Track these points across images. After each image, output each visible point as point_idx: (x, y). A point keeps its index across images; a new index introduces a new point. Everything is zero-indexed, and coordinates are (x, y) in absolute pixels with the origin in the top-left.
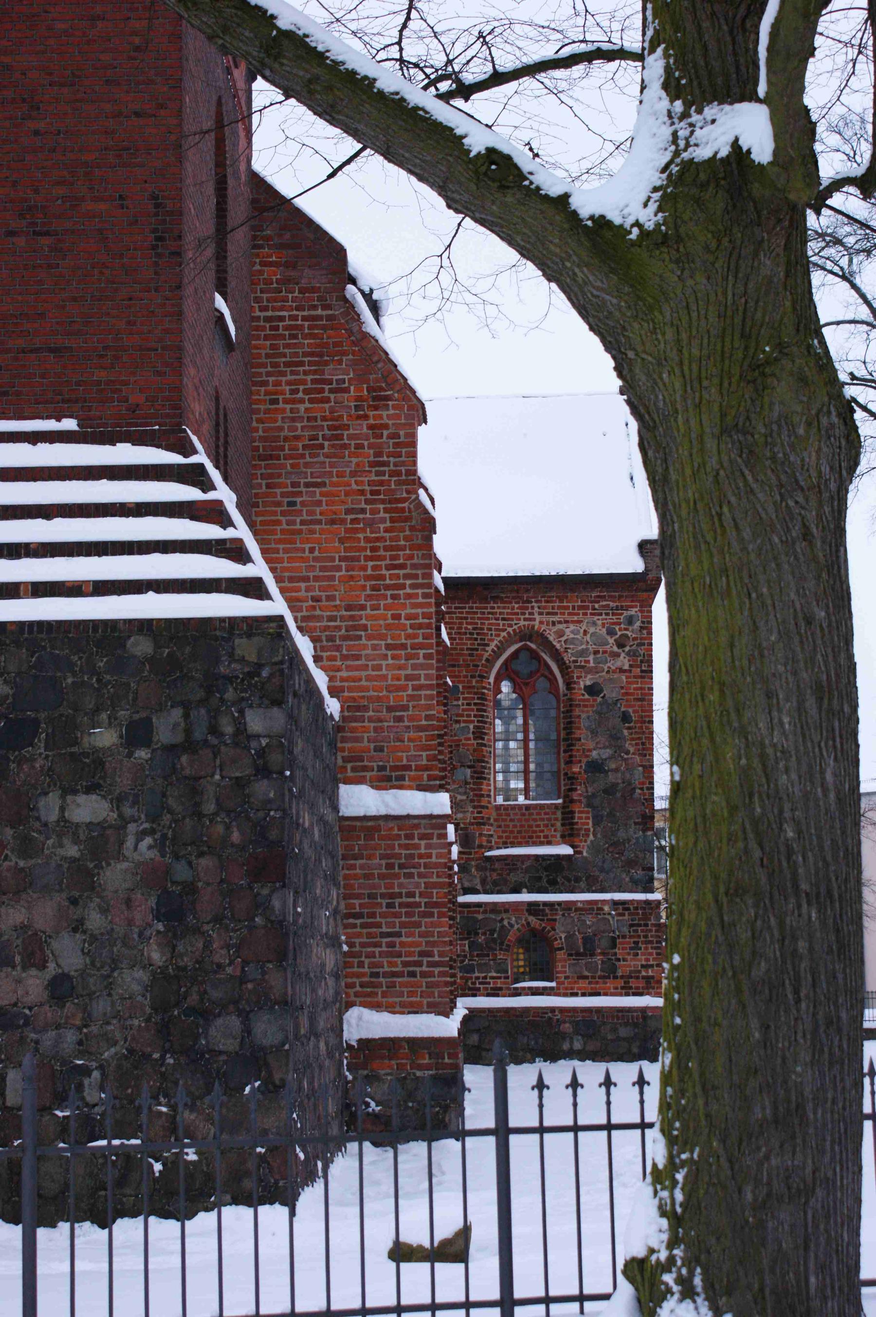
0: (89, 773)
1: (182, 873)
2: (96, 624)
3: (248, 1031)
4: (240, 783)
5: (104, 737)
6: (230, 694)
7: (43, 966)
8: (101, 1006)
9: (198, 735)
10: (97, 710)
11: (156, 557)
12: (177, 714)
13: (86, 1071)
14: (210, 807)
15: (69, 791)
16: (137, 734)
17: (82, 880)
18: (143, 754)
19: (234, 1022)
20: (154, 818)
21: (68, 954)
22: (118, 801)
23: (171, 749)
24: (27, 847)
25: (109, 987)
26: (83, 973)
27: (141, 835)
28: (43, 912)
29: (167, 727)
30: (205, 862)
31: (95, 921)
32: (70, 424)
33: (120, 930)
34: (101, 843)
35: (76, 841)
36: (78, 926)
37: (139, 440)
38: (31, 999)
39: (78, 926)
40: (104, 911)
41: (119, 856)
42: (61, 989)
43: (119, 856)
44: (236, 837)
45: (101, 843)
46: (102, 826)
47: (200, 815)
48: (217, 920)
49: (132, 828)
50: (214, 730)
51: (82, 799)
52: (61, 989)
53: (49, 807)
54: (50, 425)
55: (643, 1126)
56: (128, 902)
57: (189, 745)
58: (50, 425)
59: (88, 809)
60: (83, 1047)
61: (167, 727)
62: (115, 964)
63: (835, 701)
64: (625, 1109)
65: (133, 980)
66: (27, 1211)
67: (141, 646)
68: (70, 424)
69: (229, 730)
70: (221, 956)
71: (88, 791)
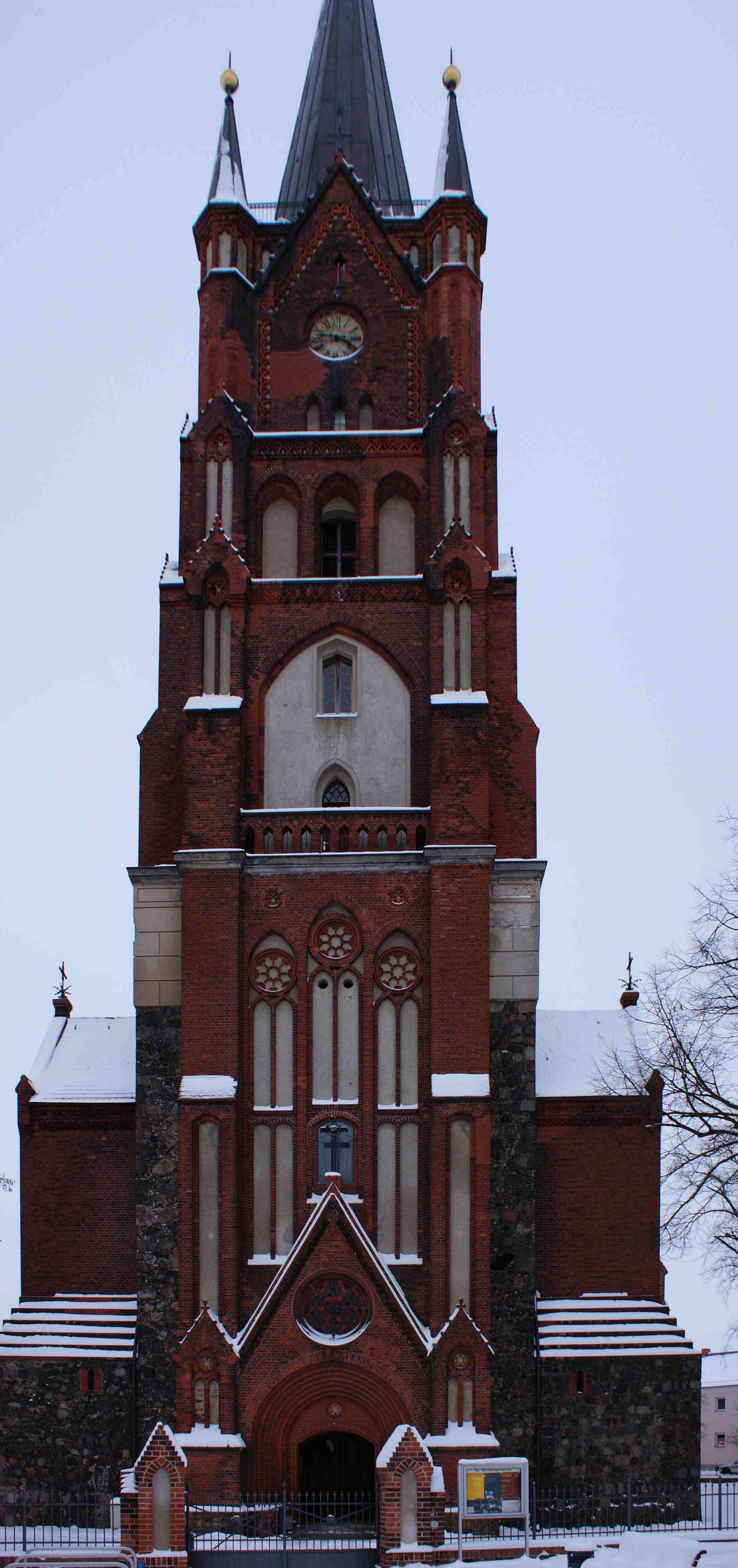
0: (643, 1400)
1: (670, 1428)
2: (645, 1357)
3: (689, 1472)
4: (688, 1403)
5: (647, 1389)
6: (686, 1376)
7: (629, 1454)
8: (646, 1466)
9: (676, 1388)
10: (646, 1381)
11: (659, 1336)
12: (669, 1383)
13: (641, 1484)
14: (679, 1410)
15: (637, 1405)
16: (657, 1389)
17: (640, 1431)
18: (659, 1394)
19: (684, 1470)
20: (663, 1413)
21: (637, 1451)
22: (652, 1409)
23: (668, 1393)
24: (624, 1421)
25: (649, 1460)
26: (641, 1457)
27: (658, 1418)
28: (630, 1439)
29: (667, 1387)
30: (677, 1425)
31: (644, 1442)
32: (625, 1294)
33: (652, 1444)
34: (647, 1420)
35: (639, 1419)
36: (639, 1443)
37: (647, 1299)
38: (625, 1464)
39: (639, 1443)
40: (647, 1439)
41: (652, 1423)
42: (634, 1461)
43: (652, 1423)
44: (687, 1418)
45: (647, 1420)
46: (647, 1415)
47: (676, 1412)
48: (681, 1441)
49: (656, 1415)
50: (681, 1387)
51: (641, 1407)
52: (634, 1461)
53: (631, 1409)
54: (619, 1295)
55: (706, 1495)
56: (655, 1437)
57: (673, 1392)
58: (619, 1295)
59: (643, 1410)
60: (641, 1477)
61: (667, 1387)
62: (650, 1454)
63: (472, 217)
64: (731, 1491)
65: (656, 1459)
66: (629, 1523)
67: (659, 1363)
68: (625, 1294)
69: (685, 1387)
70: (682, 1452)
71: (643, 1405)
